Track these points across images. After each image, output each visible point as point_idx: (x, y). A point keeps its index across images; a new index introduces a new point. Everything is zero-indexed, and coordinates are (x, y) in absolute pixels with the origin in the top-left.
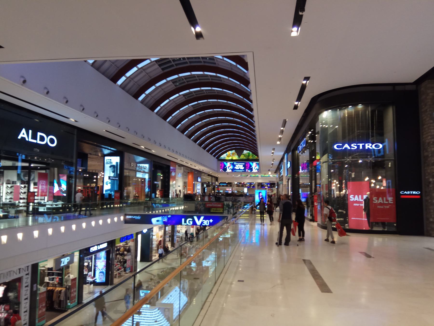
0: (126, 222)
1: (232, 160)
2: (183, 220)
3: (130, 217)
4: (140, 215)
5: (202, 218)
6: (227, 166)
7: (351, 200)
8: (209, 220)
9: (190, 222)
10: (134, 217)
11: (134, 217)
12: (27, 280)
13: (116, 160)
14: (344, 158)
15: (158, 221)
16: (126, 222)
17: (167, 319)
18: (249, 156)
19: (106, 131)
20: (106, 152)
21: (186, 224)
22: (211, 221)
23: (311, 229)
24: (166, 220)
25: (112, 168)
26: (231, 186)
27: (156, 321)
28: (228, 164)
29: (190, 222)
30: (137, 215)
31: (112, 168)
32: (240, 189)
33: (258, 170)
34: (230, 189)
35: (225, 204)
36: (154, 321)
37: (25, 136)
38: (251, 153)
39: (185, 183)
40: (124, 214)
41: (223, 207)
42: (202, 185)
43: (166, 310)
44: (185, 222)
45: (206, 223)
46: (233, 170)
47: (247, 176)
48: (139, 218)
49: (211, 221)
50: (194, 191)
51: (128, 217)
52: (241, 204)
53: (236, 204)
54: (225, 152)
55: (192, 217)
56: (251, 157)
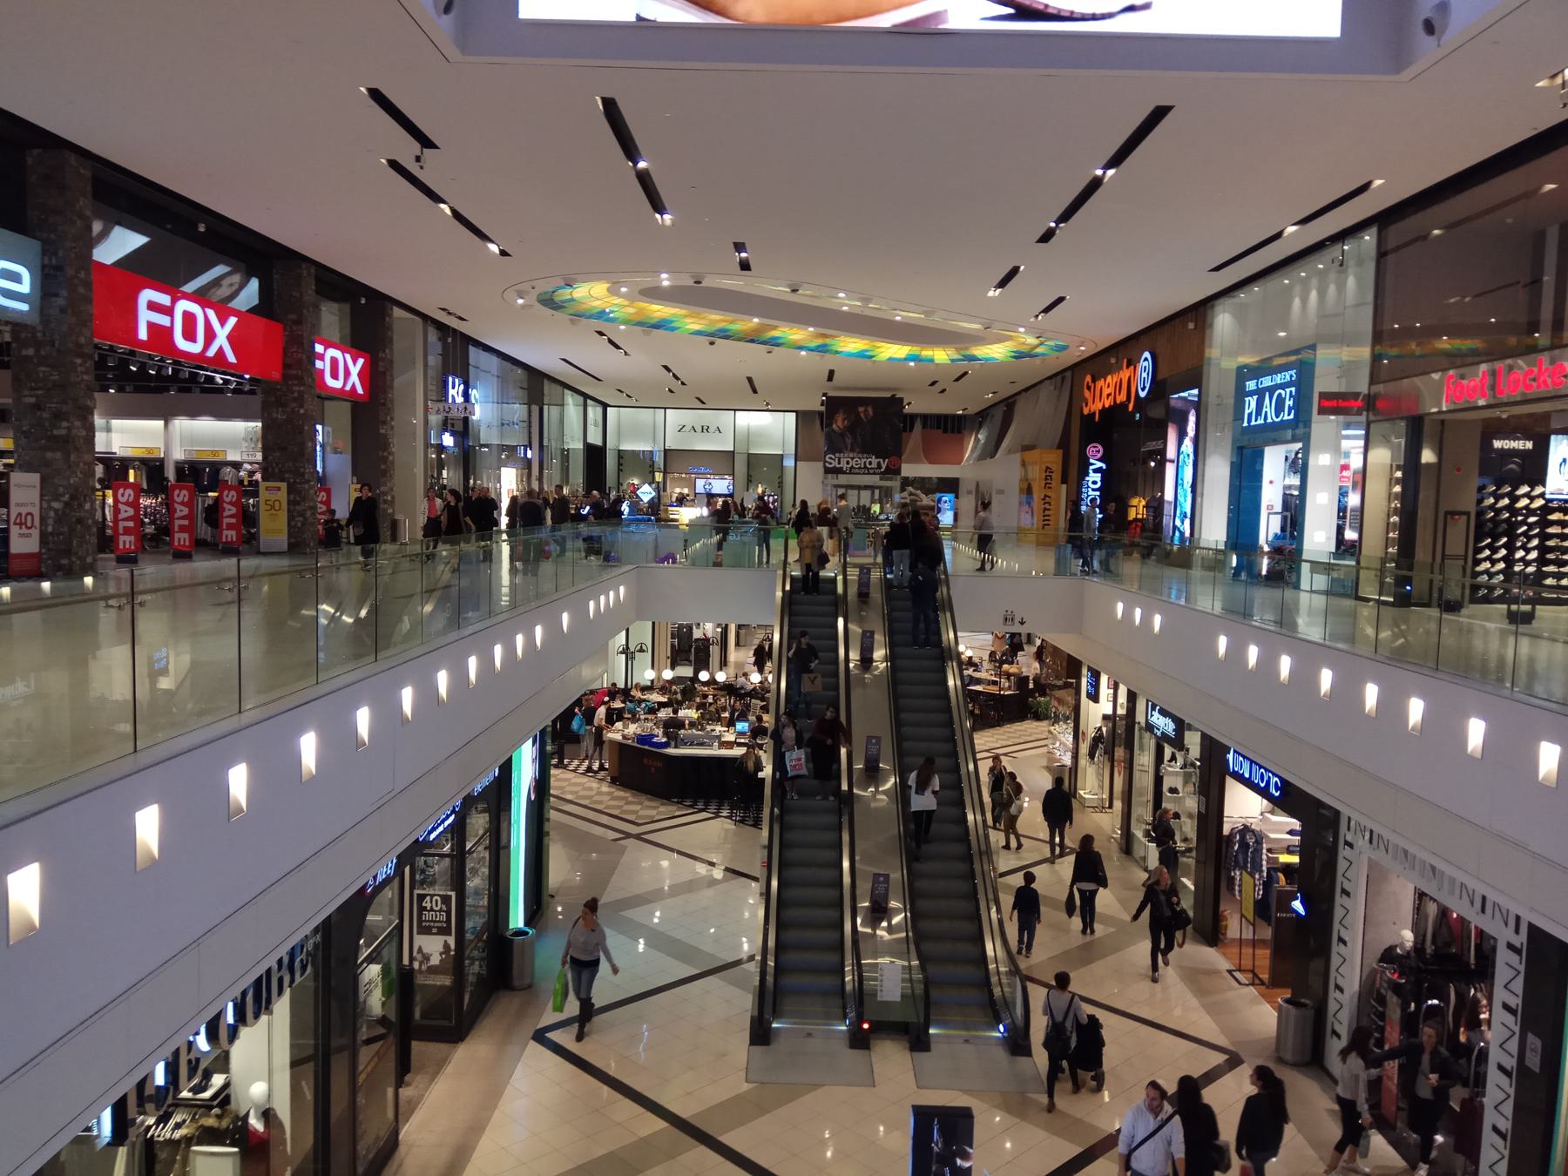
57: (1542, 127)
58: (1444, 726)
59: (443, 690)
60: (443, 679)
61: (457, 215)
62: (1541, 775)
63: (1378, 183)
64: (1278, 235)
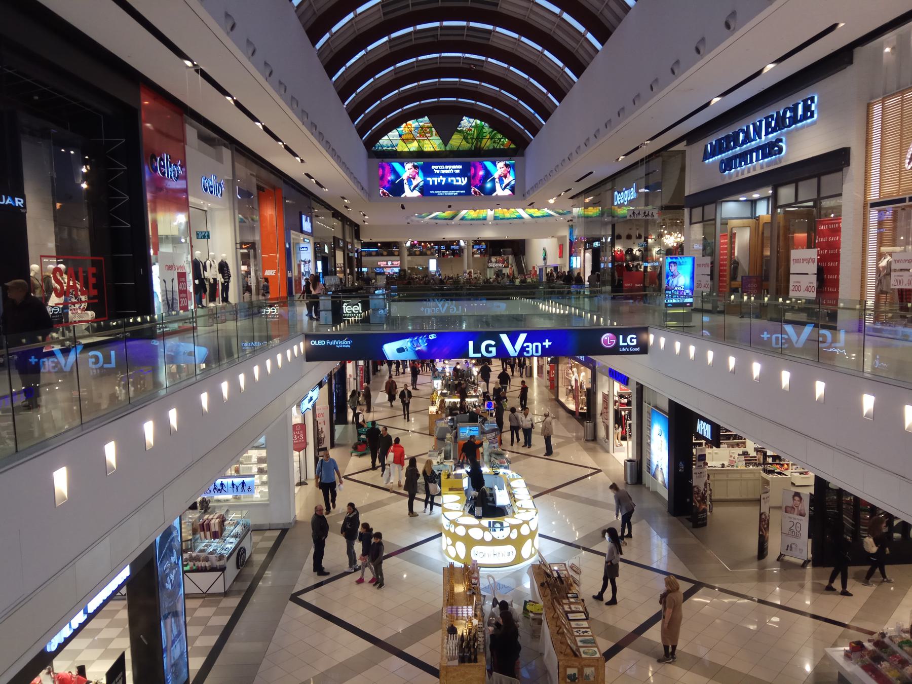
1: (420, 154)
2: (471, 343)
3: (321, 343)
4: (350, 337)
5: (522, 337)
6: (404, 176)
8: (541, 342)
9: (490, 349)
10: (333, 343)
11: (333, 343)
15: (400, 350)
18: (480, 137)
21: (479, 355)
22: (547, 343)
24: (423, 346)
26: (391, 254)
28: (407, 171)
29: (490, 349)
30: (340, 337)
33: (512, 189)
34: (397, 263)
38: (487, 129)
44: (477, 350)
46: (425, 190)
48: (346, 344)
49: (547, 343)
50: (289, 267)
51: (314, 343)
54: (395, 124)
55: (495, 336)
56: (487, 144)
57: (766, 87)
58: (771, 377)
59: (225, 394)
60: (225, 387)
61: (265, 128)
62: (906, 426)
63: (841, 25)
64: (708, 104)
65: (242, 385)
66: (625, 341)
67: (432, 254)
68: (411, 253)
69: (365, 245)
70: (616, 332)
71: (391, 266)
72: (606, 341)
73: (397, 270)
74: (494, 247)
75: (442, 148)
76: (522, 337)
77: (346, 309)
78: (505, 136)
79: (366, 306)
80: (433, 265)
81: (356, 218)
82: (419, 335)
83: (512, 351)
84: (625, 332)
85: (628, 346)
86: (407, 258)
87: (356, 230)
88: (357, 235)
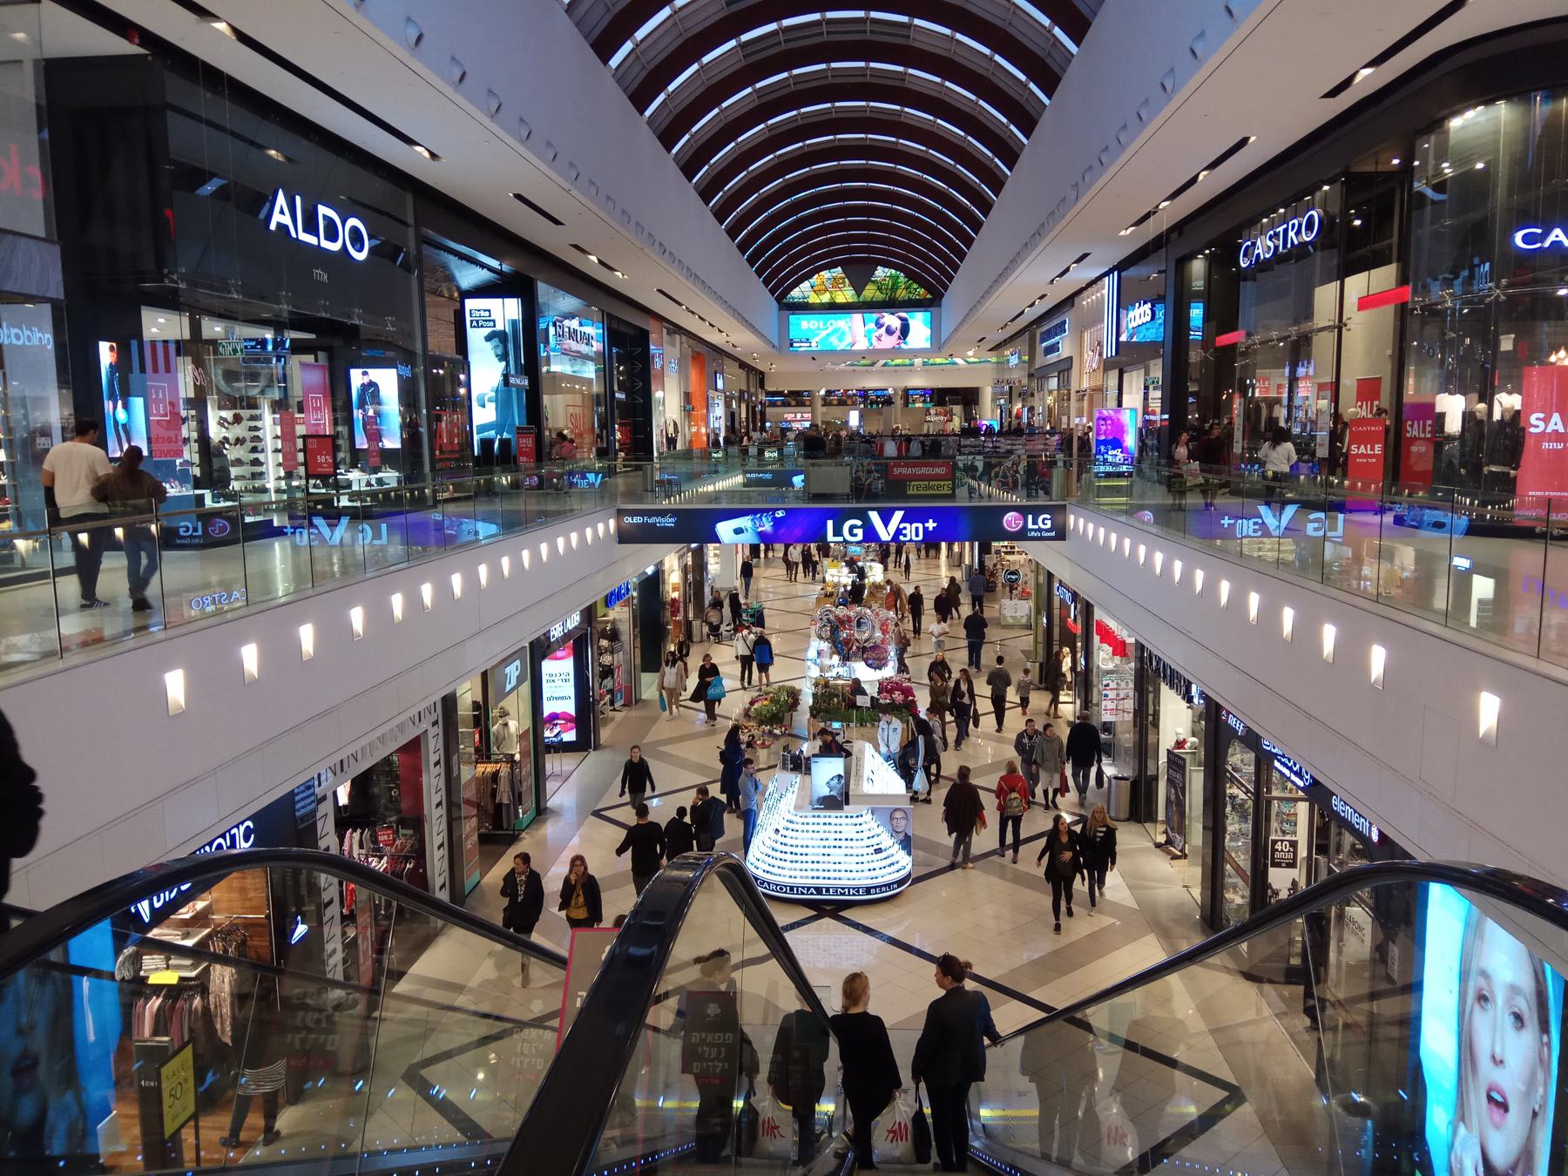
0: (625, 537)
2: (830, 523)
3: (638, 520)
5: (898, 515)
7: (1532, 430)
12: (434, 749)
13: (507, 311)
14: (1509, 296)
15: (738, 531)
16: (625, 537)
17: (901, 842)
18: (894, 288)
19: (518, 197)
20: (469, 277)
22: (931, 525)
23: (800, 575)
25: (496, 341)
26: (801, 404)
27: (878, 851)
30: (662, 513)
31: (496, 341)
32: (834, 413)
35: (961, 465)
36: (871, 850)
37: (286, 220)
38: (902, 278)
39: (687, 397)
40: (614, 511)
41: (951, 477)
42: (728, 405)
43: (898, 815)
45: (913, 532)
47: (873, 364)
48: (669, 522)
49: (931, 525)
51: (628, 520)
52: (1016, 464)
53: (1000, 464)
55: (862, 515)
56: (902, 294)
65: (526, 564)
66: (1035, 523)
67: (854, 404)
68: (826, 403)
69: (769, 394)
70: (1023, 511)
71: (800, 421)
72: (1009, 523)
73: (807, 424)
74: (941, 397)
75: (855, 299)
76: (898, 515)
77: (767, 454)
78: (921, 286)
79: (780, 451)
80: (854, 419)
81: (760, 367)
82: (762, 511)
83: (885, 535)
84: (1037, 511)
85: (1040, 530)
86: (820, 409)
87: (761, 378)
88: (762, 385)
